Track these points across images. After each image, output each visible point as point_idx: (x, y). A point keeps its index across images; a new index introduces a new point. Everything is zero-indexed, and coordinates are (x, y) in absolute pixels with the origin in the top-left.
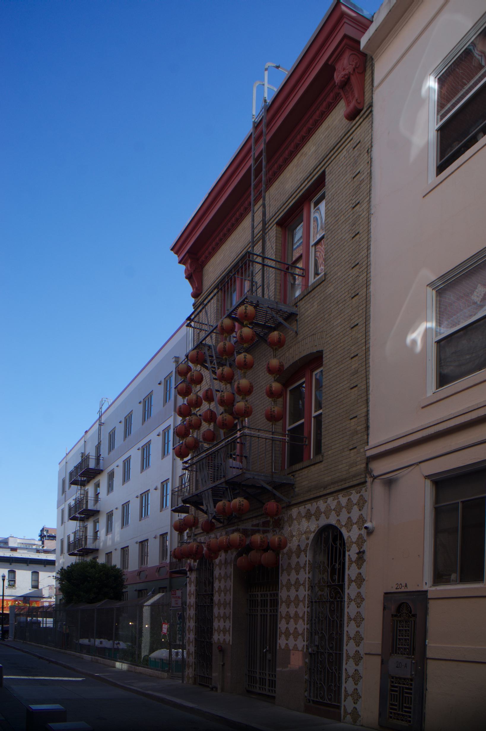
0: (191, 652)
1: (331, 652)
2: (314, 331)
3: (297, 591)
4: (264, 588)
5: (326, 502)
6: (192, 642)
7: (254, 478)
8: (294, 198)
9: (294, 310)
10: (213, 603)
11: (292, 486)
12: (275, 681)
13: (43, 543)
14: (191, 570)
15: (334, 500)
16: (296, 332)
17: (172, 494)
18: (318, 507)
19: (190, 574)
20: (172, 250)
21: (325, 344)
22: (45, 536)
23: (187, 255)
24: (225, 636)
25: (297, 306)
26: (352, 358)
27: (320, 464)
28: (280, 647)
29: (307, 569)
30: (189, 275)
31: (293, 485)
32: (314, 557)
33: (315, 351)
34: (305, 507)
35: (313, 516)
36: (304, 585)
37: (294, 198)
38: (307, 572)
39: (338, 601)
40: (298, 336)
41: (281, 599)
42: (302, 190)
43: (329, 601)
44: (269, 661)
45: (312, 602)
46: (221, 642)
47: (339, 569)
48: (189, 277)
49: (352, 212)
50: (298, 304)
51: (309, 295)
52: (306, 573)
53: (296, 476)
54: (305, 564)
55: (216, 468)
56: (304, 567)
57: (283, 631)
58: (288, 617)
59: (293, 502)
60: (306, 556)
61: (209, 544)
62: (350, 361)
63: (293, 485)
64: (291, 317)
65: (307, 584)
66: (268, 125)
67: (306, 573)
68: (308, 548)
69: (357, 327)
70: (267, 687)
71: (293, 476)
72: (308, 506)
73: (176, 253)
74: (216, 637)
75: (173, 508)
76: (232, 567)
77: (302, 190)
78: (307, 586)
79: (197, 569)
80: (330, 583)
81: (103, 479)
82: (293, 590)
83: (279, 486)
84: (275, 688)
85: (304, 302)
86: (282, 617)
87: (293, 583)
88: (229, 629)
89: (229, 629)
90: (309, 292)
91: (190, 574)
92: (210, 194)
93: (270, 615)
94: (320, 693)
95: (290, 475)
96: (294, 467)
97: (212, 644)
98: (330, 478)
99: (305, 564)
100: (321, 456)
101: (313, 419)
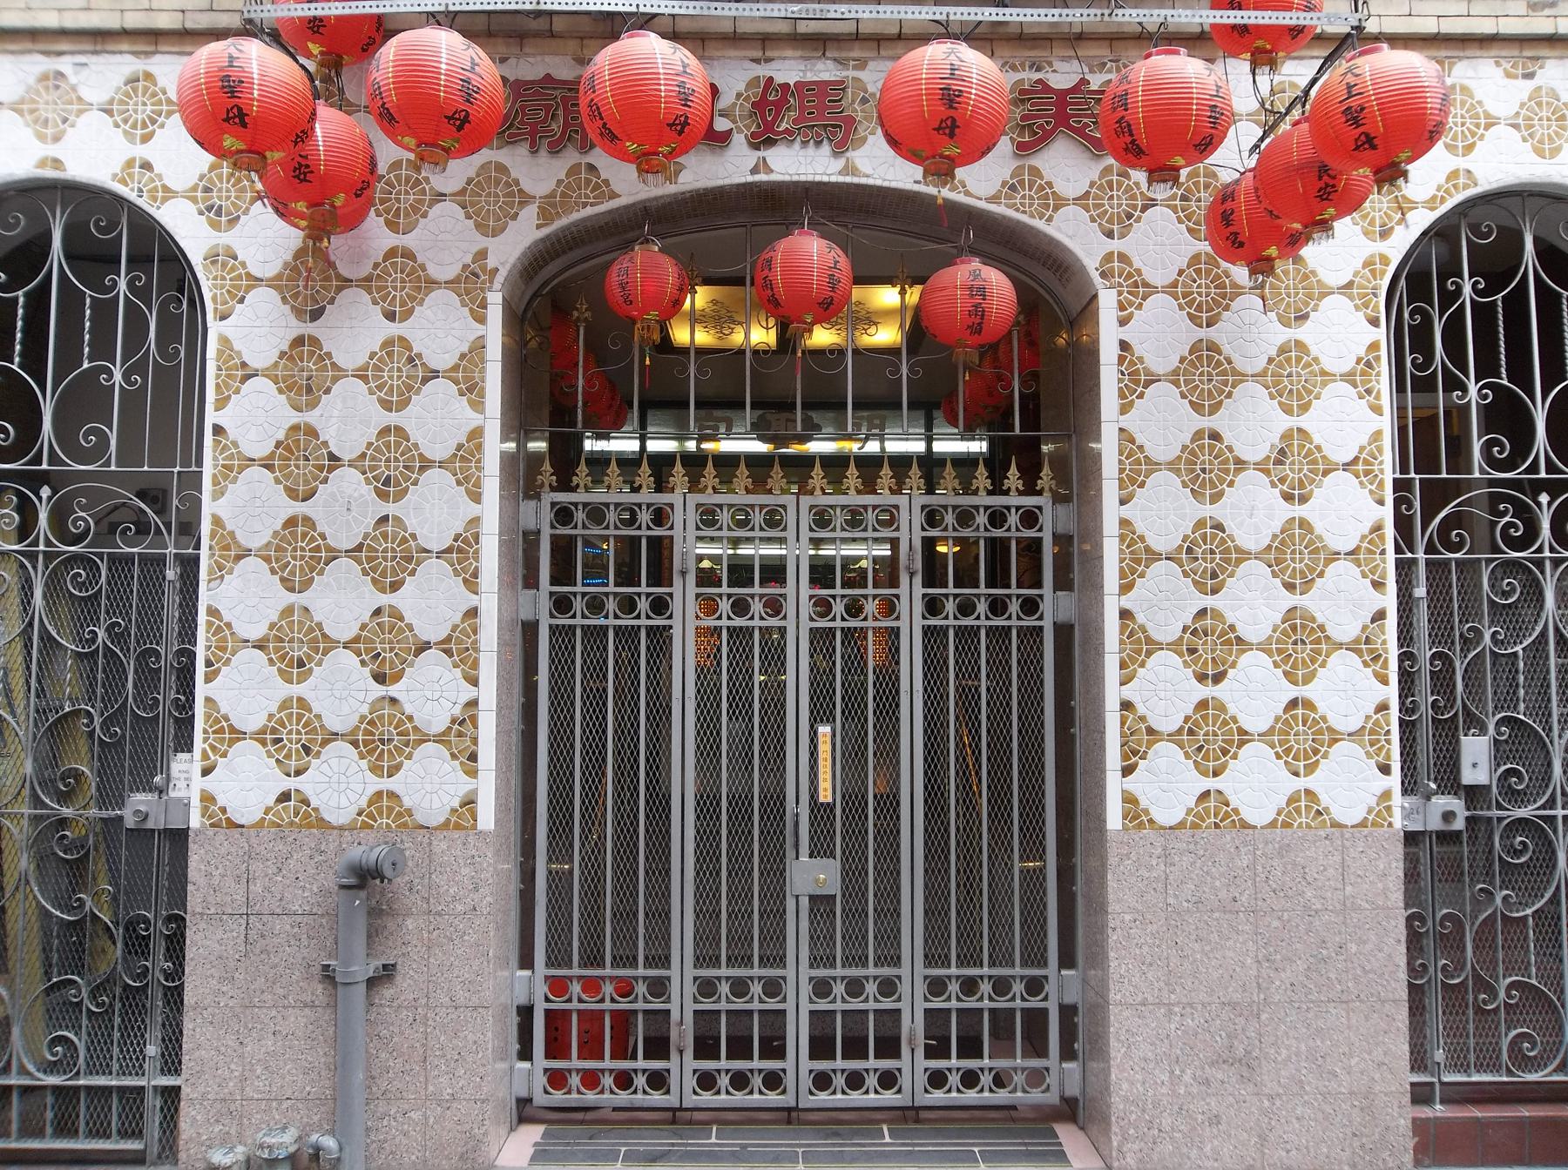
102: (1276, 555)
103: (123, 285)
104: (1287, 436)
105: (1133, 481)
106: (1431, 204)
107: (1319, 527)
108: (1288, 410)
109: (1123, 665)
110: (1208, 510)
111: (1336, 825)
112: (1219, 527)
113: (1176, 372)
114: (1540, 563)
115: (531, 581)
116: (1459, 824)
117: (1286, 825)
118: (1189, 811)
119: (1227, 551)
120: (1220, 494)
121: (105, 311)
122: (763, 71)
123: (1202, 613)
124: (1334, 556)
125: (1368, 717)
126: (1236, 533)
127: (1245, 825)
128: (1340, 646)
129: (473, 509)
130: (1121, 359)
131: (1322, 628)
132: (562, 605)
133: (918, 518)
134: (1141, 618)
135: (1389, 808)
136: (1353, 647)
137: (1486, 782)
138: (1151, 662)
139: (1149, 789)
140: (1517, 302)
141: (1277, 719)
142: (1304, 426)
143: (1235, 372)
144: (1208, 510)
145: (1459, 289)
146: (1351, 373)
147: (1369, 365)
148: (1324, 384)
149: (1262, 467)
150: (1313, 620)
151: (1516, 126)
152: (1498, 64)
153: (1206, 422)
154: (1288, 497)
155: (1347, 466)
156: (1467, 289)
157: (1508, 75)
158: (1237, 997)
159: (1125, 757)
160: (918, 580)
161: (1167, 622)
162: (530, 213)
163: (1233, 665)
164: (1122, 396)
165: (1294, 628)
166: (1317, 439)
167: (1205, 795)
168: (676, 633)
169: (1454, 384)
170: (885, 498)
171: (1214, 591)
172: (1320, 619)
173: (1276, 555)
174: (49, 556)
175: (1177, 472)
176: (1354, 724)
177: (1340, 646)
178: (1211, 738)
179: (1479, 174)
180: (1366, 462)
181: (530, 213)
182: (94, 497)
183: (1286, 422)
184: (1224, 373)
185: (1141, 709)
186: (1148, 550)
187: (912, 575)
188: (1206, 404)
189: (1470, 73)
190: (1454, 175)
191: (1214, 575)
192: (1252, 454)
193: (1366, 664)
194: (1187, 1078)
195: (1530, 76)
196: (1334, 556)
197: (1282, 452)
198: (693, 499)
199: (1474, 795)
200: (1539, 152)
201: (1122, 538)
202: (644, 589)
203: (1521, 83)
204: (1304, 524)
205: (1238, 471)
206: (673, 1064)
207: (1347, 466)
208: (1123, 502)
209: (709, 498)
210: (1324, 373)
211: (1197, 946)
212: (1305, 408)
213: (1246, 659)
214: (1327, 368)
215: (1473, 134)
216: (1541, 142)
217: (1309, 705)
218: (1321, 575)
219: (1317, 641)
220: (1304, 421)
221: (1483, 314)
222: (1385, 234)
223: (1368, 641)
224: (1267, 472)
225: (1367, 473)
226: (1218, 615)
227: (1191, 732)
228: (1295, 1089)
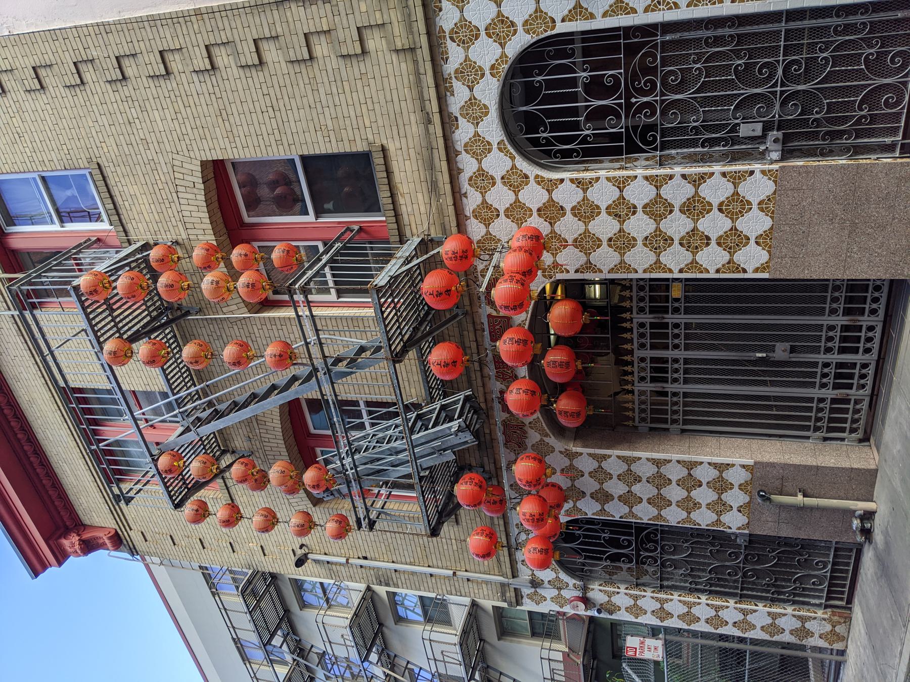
1: (742, 557)
4: (625, 320)
12: (848, 280)
21: (192, 155)
23: (51, 542)
39: (662, 539)
43: (661, 554)
44: (793, 350)
47: (612, 532)
61: (527, 482)
70: (859, 358)
73: (45, 567)
80: (632, 550)
84: (869, 280)
86: (688, 519)
90: (115, 208)
93: (686, 381)
94: (814, 583)
102: (658, 217)
103: (539, 78)
104: (609, 214)
105: (628, 269)
106: (513, 158)
107: (646, 201)
108: (599, 213)
109: (701, 272)
110: (640, 242)
111: (775, 193)
112: (646, 238)
113: (586, 254)
114: (663, 101)
115: (667, 430)
116: (780, 134)
117: (773, 213)
118: (763, 249)
119: (656, 235)
120: (633, 238)
121: (550, 84)
122: (493, 378)
123: (681, 244)
124: (658, 195)
125: (728, 181)
126: (649, 232)
127: (771, 228)
128: (696, 192)
129: (640, 10)
130: (582, 272)
131: (688, 199)
132: (674, 421)
133: (643, 384)
134: (682, 266)
135: (769, 171)
136: (697, 187)
137: (761, 124)
138: (701, 263)
139: (752, 261)
140: (549, 113)
141: (726, 216)
142: (605, 207)
143: (585, 233)
144: (640, 242)
145: (545, 138)
146: (583, 189)
147: (579, 183)
148: (588, 200)
149: (622, 223)
150: (685, 203)
151: (478, 124)
152: (454, 132)
153: (605, 243)
154: (634, 213)
155: (621, 191)
156: (545, 135)
157: (457, 128)
158: (846, 232)
159: (739, 272)
160: (666, 316)
161: (685, 257)
162: (546, 439)
163: (703, 233)
164: (596, 272)
165: (688, 210)
166: (610, 202)
167: (757, 243)
168: (685, 390)
169: (584, 140)
170: (635, 326)
171: (672, 240)
172: (684, 200)
173: (658, 217)
174: (663, 94)
175: (624, 253)
176: (731, 186)
177: (696, 192)
178: (733, 240)
179: (499, 139)
180: (619, 183)
181: (546, 439)
182: (635, 77)
183: (604, 214)
184: (585, 237)
185: (720, 266)
186: (655, 263)
187: (664, 318)
188: (598, 243)
189: (459, 143)
190: (500, 149)
191: (666, 240)
192: (617, 227)
193: (705, 182)
194: (879, 251)
195: (456, 118)
196: (658, 195)
197: (616, 215)
198: (636, 383)
199: (767, 127)
200: (487, 114)
201: (651, 272)
202: (670, 331)
203: (460, 122)
204: (645, 207)
205: (624, 232)
206: (864, 324)
207: (621, 191)
208: (637, 272)
209: (636, 379)
210: (583, 200)
211: (822, 246)
212: (598, 207)
213: (700, 228)
214: (582, 198)
215: (483, 142)
216: (482, 113)
217: (721, 204)
218: (666, 200)
219: (694, 201)
220: (603, 207)
221: (555, 127)
222: (527, 177)
223: (695, 181)
224: (624, 221)
225: (624, 183)
226: (682, 239)
227: (730, 248)
228: (892, 209)
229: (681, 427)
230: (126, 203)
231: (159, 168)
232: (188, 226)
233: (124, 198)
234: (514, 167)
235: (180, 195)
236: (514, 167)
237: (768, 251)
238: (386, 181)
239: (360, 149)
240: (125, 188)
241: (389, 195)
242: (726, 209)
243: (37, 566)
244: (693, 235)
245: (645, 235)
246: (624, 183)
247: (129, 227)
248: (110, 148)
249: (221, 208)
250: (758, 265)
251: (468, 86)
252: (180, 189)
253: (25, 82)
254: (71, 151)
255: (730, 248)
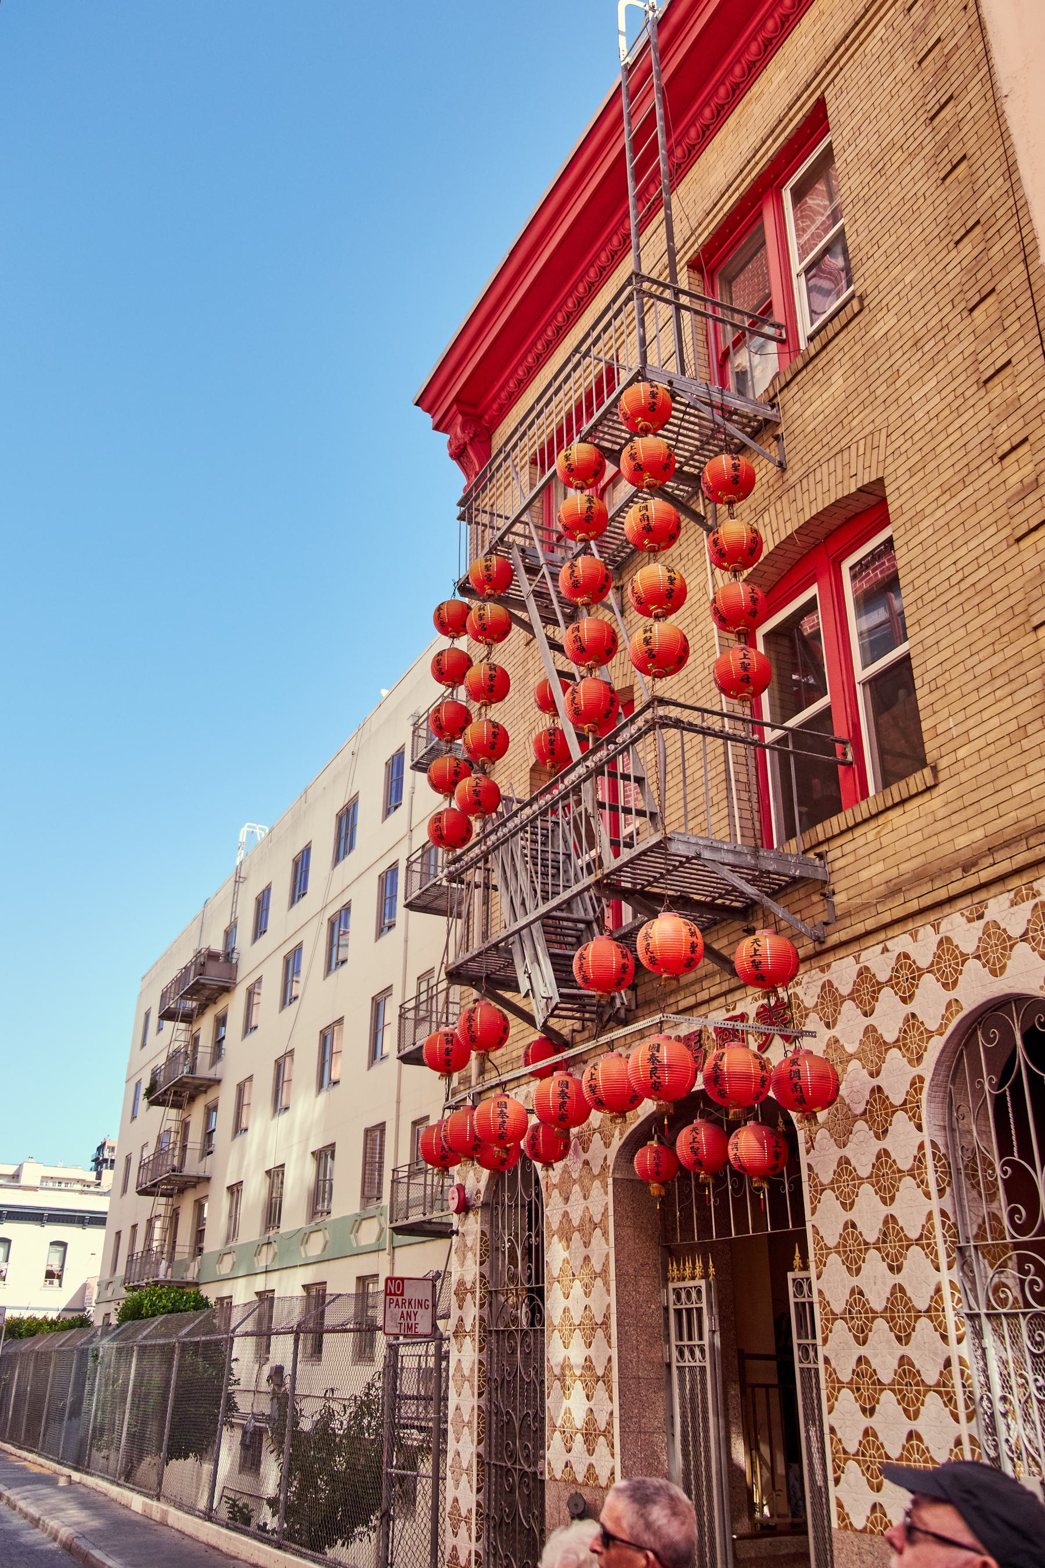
0: (464, 1512)
2: (843, 443)
3: (895, 1269)
5: (980, 917)
6: (468, 1469)
7: (698, 857)
8: (737, 189)
9: (769, 413)
10: (542, 1322)
11: (823, 888)
13: (99, 1176)
14: (464, 1207)
15: (1013, 904)
16: (781, 465)
17: (393, 1181)
18: (945, 942)
19: (463, 1222)
20: (417, 404)
21: (890, 460)
22: (105, 1161)
23: (455, 407)
24: (591, 1452)
25: (773, 406)
26: (1002, 458)
27: (927, 797)
28: (843, 1517)
29: (931, 1177)
30: (458, 447)
31: (825, 882)
32: (950, 1128)
33: (853, 490)
34: (885, 950)
35: (928, 978)
36: (924, 1241)
37: (737, 189)
38: (933, 1189)
39: (535, 1331)
40: (789, 473)
41: (825, 1305)
42: (757, 163)
45: (973, 1317)
46: (580, 1479)
48: (458, 454)
49: (929, 129)
50: (779, 398)
51: (810, 367)
52: (927, 1195)
53: (830, 856)
54: (920, 1160)
55: (550, 871)
56: (916, 1171)
57: (852, 1447)
58: (866, 1384)
59: (833, 939)
60: (919, 1128)
62: (998, 467)
63: (825, 882)
64: (763, 428)
65: (940, 1240)
66: (664, 52)
67: (927, 1195)
68: (924, 1096)
69: (1008, 370)
71: (820, 856)
72: (900, 943)
73: (428, 410)
74: (556, 1457)
75: (403, 1053)
76: (610, 1188)
77: (757, 163)
78: (941, 1249)
79: (485, 1205)
80: (1013, 1237)
81: (235, 1004)
82: (874, 1264)
83: (784, 888)
85: (796, 389)
87: (871, 1236)
88: (610, 1424)
89: (610, 1424)
91: (463, 1222)
92: (513, 253)
95: (811, 855)
96: (819, 827)
97: (542, 1482)
98: (979, 834)
99: (920, 1160)
100: (927, 771)
101: (859, 689)
147: (920, 1161)
229: (674, 1365)
230: (820, 374)
231: (867, 411)
232: (805, 481)
233: (826, 369)
234: (930, 1034)
235: (839, 456)
236: (930, 1034)
237: (865, 1528)
238: (889, 803)
239: (928, 747)
240: (838, 366)
241: (873, 812)
242: (912, 1446)
243: (427, 401)
244: (873, 1383)
245: (865, 1291)
246: (929, 1245)
247: (794, 388)
248: (882, 323)
249: (848, 520)
250: (847, 1509)
251: (1026, 933)
252: (846, 453)
253: (946, 151)
254: (871, 261)
255: (864, 1455)
